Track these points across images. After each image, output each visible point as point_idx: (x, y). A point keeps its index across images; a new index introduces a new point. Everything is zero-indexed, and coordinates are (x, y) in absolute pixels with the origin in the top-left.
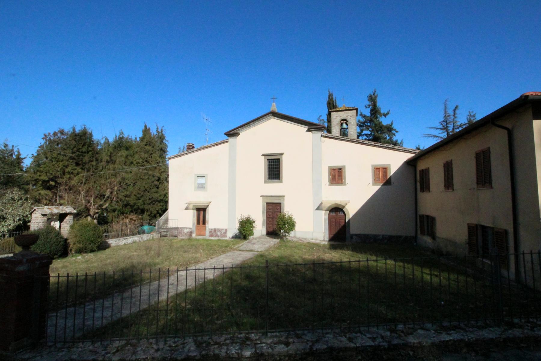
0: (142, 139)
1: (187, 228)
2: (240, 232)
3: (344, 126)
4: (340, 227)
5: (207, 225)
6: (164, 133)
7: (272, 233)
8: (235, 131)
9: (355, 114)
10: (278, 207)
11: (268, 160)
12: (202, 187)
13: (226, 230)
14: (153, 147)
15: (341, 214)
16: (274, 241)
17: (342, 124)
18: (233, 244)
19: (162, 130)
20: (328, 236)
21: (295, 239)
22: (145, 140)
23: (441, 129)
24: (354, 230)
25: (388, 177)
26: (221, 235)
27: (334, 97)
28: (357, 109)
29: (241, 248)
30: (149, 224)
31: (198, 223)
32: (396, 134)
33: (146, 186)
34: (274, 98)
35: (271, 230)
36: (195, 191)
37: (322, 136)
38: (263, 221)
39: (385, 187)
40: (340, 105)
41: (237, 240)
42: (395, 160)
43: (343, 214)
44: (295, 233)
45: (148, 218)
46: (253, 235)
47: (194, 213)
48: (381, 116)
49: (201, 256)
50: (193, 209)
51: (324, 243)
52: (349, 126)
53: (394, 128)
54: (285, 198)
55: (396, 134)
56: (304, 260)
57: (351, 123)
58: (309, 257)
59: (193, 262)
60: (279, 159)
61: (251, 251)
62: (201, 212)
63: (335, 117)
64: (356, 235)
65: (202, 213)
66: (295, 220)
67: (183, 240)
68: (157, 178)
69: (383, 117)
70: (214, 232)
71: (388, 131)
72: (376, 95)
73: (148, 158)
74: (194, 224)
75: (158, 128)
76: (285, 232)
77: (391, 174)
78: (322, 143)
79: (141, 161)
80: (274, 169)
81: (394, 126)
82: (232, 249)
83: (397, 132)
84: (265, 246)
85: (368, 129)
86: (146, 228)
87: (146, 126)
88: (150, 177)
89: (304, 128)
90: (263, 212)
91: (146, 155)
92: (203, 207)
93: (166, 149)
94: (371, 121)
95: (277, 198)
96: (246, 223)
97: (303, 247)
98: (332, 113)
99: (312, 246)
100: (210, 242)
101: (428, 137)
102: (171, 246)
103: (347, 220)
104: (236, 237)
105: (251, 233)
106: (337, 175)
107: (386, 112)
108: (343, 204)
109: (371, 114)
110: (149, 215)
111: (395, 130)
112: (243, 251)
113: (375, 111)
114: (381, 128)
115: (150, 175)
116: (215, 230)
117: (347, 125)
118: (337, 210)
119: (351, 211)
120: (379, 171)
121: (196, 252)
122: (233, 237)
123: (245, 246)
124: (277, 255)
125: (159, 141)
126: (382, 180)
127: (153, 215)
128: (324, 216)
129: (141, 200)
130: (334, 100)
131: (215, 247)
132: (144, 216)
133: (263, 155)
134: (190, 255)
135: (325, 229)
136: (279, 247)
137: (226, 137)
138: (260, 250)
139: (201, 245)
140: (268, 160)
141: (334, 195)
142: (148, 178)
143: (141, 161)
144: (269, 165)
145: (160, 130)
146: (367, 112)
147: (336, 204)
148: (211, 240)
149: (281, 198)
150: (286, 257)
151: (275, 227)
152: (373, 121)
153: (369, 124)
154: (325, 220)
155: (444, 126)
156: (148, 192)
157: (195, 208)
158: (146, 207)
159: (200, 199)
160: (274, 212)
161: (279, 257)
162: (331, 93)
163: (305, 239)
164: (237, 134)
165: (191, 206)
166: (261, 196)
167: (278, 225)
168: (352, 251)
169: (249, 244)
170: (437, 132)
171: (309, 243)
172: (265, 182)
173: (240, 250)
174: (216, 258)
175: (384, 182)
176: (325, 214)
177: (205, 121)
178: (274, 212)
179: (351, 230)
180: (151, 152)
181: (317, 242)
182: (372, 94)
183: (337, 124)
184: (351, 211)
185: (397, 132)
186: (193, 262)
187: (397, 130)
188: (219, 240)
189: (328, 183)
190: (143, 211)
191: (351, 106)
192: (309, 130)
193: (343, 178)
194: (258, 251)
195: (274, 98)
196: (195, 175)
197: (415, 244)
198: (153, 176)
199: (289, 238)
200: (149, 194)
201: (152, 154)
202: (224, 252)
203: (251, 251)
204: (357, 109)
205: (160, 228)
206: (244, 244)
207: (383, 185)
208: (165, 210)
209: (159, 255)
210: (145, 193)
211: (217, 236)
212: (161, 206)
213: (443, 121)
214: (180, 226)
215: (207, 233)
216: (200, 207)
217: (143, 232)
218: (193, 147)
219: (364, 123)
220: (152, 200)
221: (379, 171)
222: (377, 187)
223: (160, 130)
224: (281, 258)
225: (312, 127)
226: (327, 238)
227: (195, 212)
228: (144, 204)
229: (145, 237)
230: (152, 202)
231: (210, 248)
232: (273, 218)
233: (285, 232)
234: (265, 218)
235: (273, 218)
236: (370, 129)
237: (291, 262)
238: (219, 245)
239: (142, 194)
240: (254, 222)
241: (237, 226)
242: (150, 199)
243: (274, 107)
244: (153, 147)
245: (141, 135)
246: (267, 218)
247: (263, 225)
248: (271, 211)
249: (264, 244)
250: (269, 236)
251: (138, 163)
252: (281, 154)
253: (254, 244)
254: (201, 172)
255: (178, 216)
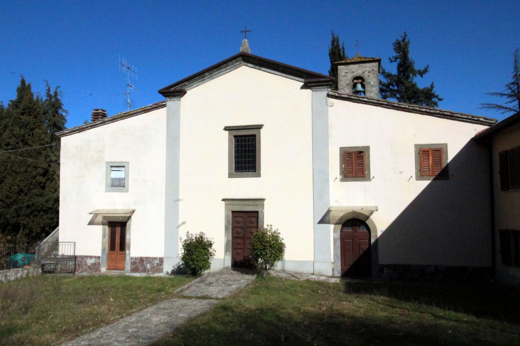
0: (15, 104)
1: (91, 257)
2: (186, 263)
3: (359, 87)
4: (362, 252)
5: (127, 252)
6: (59, 97)
7: (242, 265)
8: (178, 88)
9: (376, 69)
10: (253, 219)
11: (235, 137)
12: (119, 185)
13: (161, 260)
14: (35, 117)
15: (362, 230)
16: (245, 280)
17: (355, 86)
18: (173, 286)
19: (56, 93)
20: (339, 268)
21: (283, 275)
22: (22, 106)
23: (510, 96)
24: (384, 258)
25: (444, 165)
26: (153, 268)
27: (340, 43)
28: (379, 61)
29: (187, 293)
30: (27, 251)
31: (112, 247)
32: (439, 103)
33: (22, 185)
34: (246, 32)
35: (240, 258)
36: (107, 191)
37: (328, 96)
38: (227, 244)
39: (439, 182)
40: (350, 54)
41: (180, 278)
42: (455, 137)
43: (365, 230)
44: (283, 264)
45: (26, 240)
46: (209, 267)
47: (104, 231)
48: (414, 74)
49: (109, 310)
50: (103, 224)
51: (333, 280)
52: (368, 88)
53: (436, 94)
54: (265, 203)
55: (439, 103)
56: (306, 314)
57: (369, 83)
58: (312, 309)
59: (90, 323)
60: (254, 136)
61: (205, 297)
62: (117, 228)
63: (343, 74)
64: (389, 266)
65: (118, 230)
66: (283, 241)
67: (83, 278)
68: (41, 171)
69: (418, 76)
70: (140, 263)
71: (426, 98)
72: (406, 40)
73: (27, 136)
74: (103, 250)
75: (49, 90)
76: (266, 262)
77: (449, 160)
78: (330, 108)
79: (13, 141)
80: (245, 152)
81: (436, 91)
82: (169, 296)
83: (440, 100)
84: (230, 288)
85: (395, 95)
86: (20, 257)
87: (23, 82)
88: (30, 169)
89: (298, 84)
90: (227, 228)
91: (22, 132)
92: (121, 220)
93: (63, 124)
94: (399, 82)
95: (251, 203)
96: (196, 247)
97: (299, 289)
98: (340, 67)
99: (315, 287)
100: (130, 281)
101: (489, 108)
102: (57, 290)
103: (373, 241)
104: (178, 272)
105: (206, 265)
106: (355, 164)
107: (422, 69)
108: (366, 213)
109: (399, 72)
110: (27, 235)
111: (437, 97)
112: (190, 298)
113: (405, 67)
114: (415, 93)
115: (29, 166)
116: (142, 259)
117: (363, 86)
118: (354, 224)
119: (381, 222)
120: (428, 156)
121: (102, 302)
122: (173, 273)
123: (193, 288)
124: (253, 307)
125: (50, 112)
126: (433, 173)
127: (34, 234)
128: (331, 233)
129: (12, 210)
130: (341, 47)
131: (139, 292)
132: (19, 236)
133: (226, 129)
134: (88, 309)
135: (335, 255)
136: (254, 290)
137: (161, 98)
138: (220, 296)
139: (113, 287)
140: (235, 137)
141: (349, 197)
142: (26, 171)
143: (13, 141)
144: (237, 146)
145: (52, 93)
146: (393, 69)
147: (354, 212)
148: (135, 278)
149: (258, 203)
150: (270, 309)
151: (247, 253)
152: (402, 83)
153: (396, 88)
154: (335, 240)
155: (513, 91)
156: (26, 195)
157: (106, 221)
158: (23, 221)
159: (116, 204)
160: (245, 222)
161: (257, 309)
162: (336, 36)
163: (300, 274)
164: (181, 93)
165: (100, 219)
166: (223, 200)
167: (254, 249)
168: (388, 296)
169: (202, 285)
170: (503, 101)
171: (308, 281)
172: (231, 176)
173: (185, 297)
174: (138, 314)
175: (437, 173)
176: (335, 231)
177: (124, 69)
178: (245, 222)
179: (380, 258)
180: (31, 126)
181: (322, 278)
182: (401, 39)
183: (347, 84)
184: (381, 222)
185: (440, 100)
186: (90, 323)
187: (440, 97)
188: (146, 278)
189: (339, 177)
190: (16, 228)
191: (371, 55)
192: (305, 86)
193: (366, 167)
194: (217, 299)
195: (246, 32)
196: (107, 163)
197: (492, 281)
198: (35, 168)
199: (273, 273)
200: (26, 198)
201: (32, 129)
202: (153, 301)
203: (205, 297)
204: (379, 61)
205: (45, 257)
206: (193, 286)
207: (434, 179)
208: (54, 224)
209: (27, 309)
210: (20, 197)
211: (145, 270)
212: (47, 216)
213: (513, 83)
214: (79, 253)
215: (128, 267)
216: (115, 220)
217: (15, 265)
218: (104, 116)
219: (388, 86)
220: (33, 208)
221: (428, 156)
222: (425, 184)
223: (52, 93)
224: (262, 311)
225: (311, 80)
226: (338, 273)
227: (107, 227)
228: (19, 216)
229: (13, 274)
230: (32, 212)
231: (129, 293)
232: (243, 238)
233: (266, 262)
234: (230, 239)
235: (243, 238)
236: (398, 96)
237: (280, 319)
238: (147, 288)
239: (14, 198)
240: (210, 245)
241: (181, 252)
242: (28, 207)
243: (245, 46)
244: (35, 117)
245: (14, 97)
246: (234, 238)
247: (226, 250)
248: (241, 225)
249: (229, 285)
250: (238, 271)
251: (8, 145)
252: (259, 127)
253: (210, 284)
254: (118, 159)
255: (78, 236)
